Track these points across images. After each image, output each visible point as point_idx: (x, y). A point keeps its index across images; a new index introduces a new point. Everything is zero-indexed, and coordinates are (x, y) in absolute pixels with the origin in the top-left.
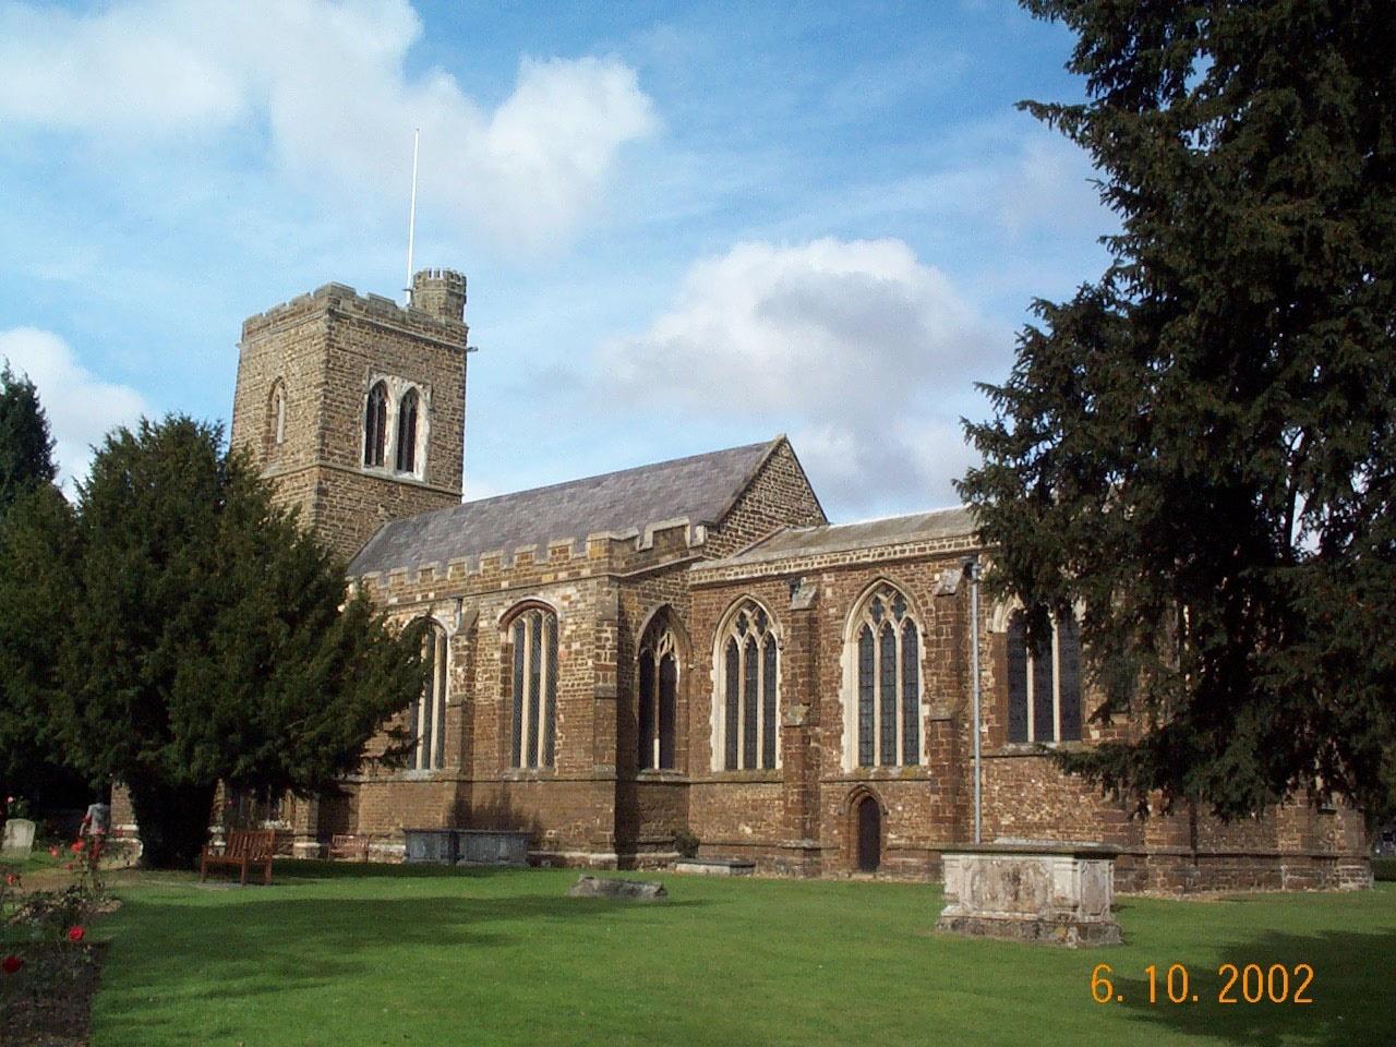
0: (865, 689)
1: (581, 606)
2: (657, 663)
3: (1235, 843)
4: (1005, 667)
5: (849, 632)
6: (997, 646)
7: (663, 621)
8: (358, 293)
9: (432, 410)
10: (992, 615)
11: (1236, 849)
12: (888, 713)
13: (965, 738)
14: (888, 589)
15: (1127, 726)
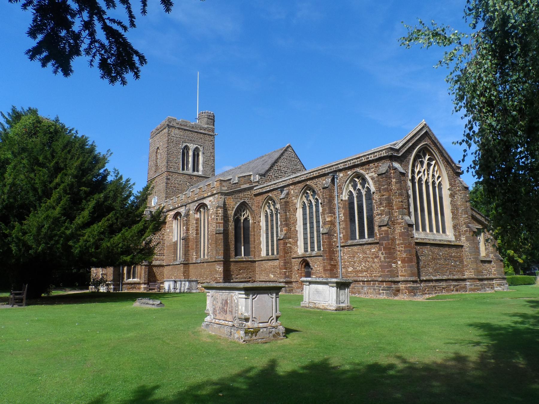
0: (305, 224)
1: (214, 203)
2: (242, 221)
3: (445, 275)
4: (348, 212)
5: (299, 205)
6: (344, 205)
7: (244, 207)
9: (203, 153)
10: (342, 194)
11: (445, 277)
12: (312, 233)
13: (335, 239)
15: (387, 231)
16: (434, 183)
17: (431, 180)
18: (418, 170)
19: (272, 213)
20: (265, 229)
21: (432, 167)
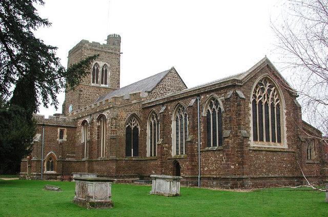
5: (173, 119)
8: (101, 44)
14: (214, 99)
16: (272, 105)
17: (270, 103)
18: (259, 95)
19: (155, 123)
20: (150, 136)
21: (271, 93)
